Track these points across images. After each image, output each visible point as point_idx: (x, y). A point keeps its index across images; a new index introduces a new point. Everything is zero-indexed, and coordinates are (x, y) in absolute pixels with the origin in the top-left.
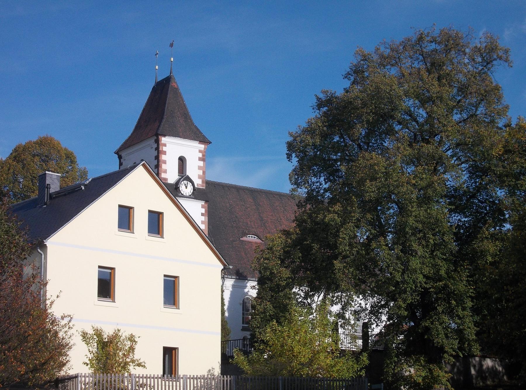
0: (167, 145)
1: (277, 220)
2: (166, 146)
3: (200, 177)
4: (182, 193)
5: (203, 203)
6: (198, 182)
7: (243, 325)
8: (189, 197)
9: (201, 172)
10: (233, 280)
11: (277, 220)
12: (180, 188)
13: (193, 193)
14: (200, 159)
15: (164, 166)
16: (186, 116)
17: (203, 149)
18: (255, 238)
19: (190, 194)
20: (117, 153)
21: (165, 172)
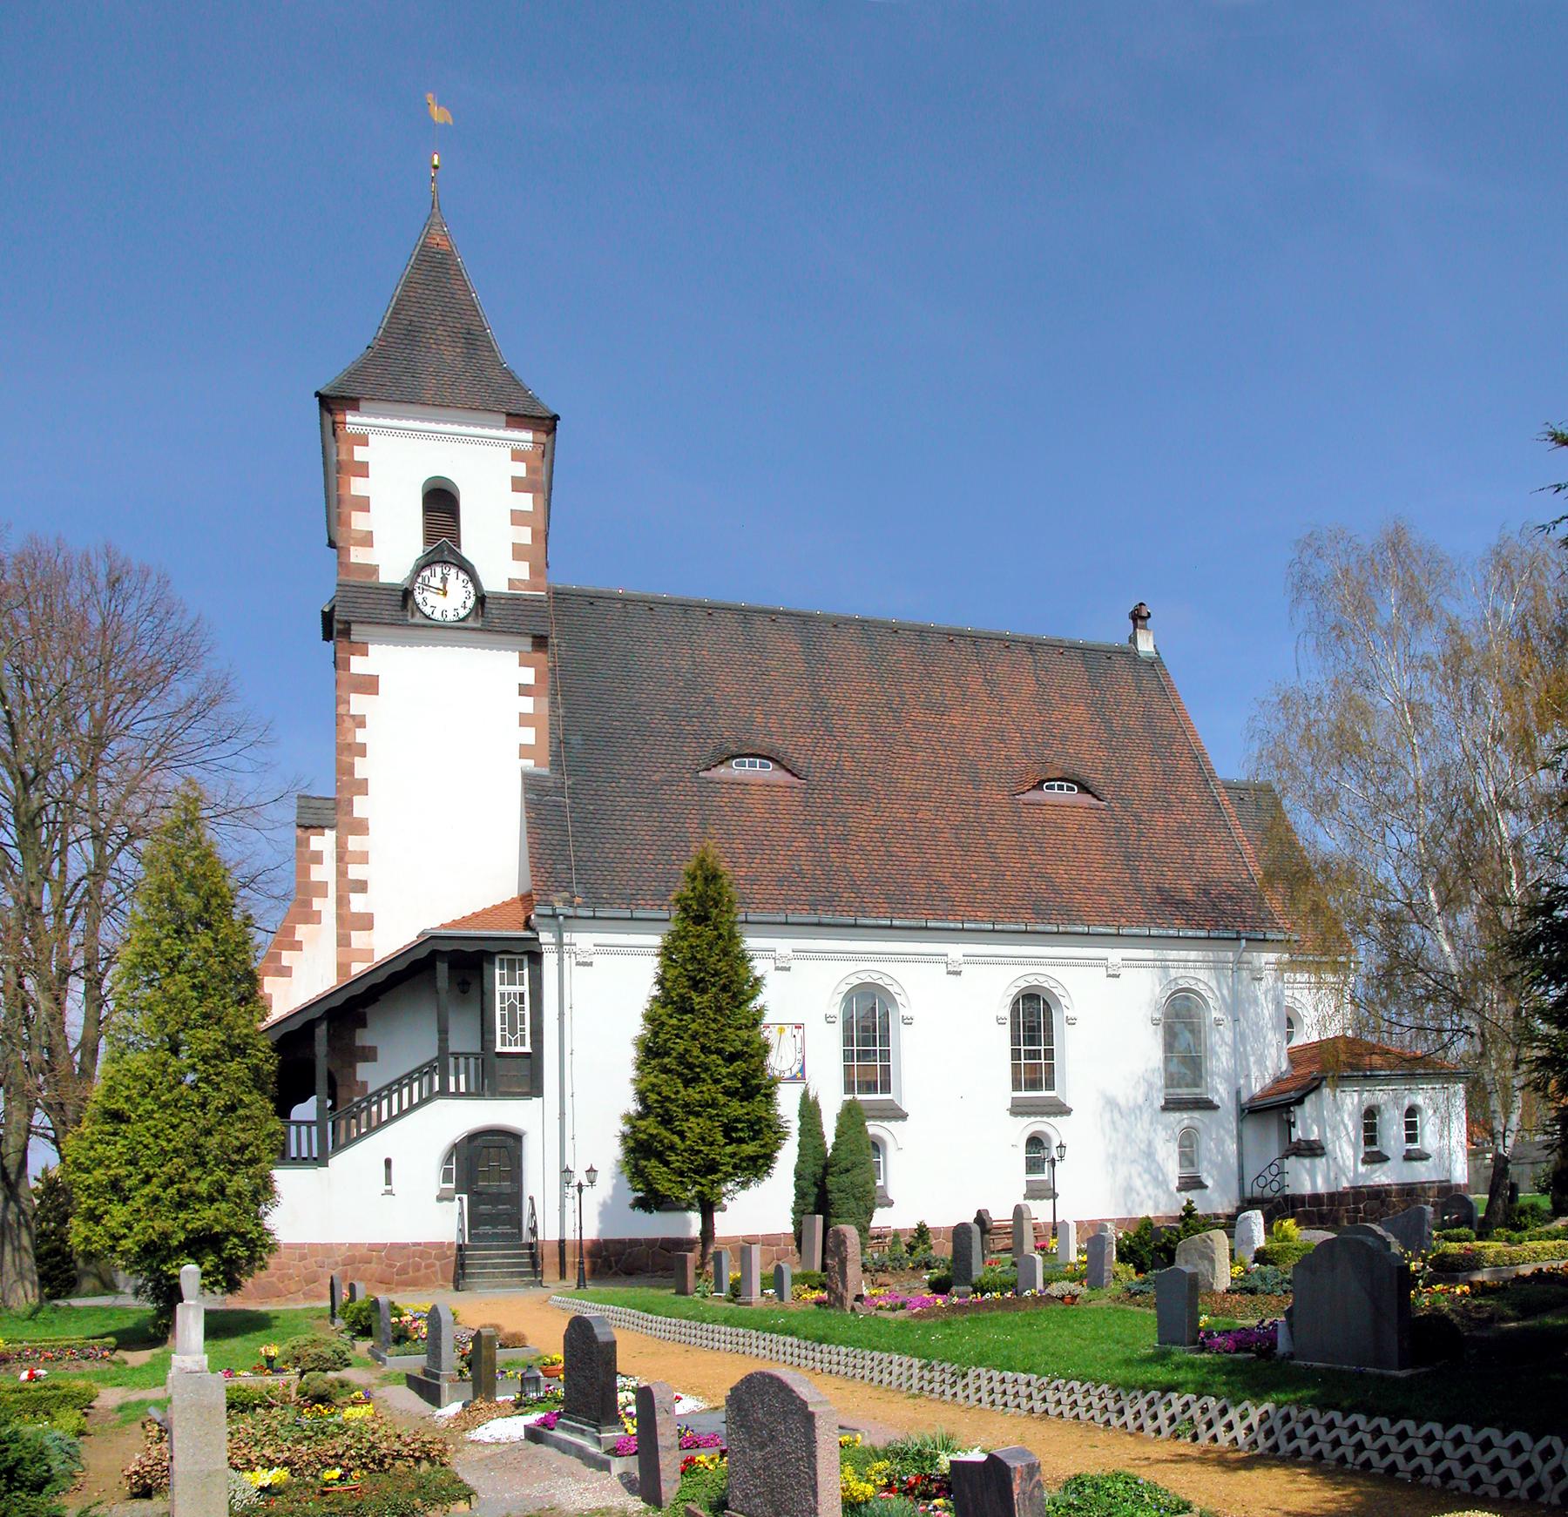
4: (427, 610)
16: (474, 340)
19: (463, 613)
21: (367, 540)
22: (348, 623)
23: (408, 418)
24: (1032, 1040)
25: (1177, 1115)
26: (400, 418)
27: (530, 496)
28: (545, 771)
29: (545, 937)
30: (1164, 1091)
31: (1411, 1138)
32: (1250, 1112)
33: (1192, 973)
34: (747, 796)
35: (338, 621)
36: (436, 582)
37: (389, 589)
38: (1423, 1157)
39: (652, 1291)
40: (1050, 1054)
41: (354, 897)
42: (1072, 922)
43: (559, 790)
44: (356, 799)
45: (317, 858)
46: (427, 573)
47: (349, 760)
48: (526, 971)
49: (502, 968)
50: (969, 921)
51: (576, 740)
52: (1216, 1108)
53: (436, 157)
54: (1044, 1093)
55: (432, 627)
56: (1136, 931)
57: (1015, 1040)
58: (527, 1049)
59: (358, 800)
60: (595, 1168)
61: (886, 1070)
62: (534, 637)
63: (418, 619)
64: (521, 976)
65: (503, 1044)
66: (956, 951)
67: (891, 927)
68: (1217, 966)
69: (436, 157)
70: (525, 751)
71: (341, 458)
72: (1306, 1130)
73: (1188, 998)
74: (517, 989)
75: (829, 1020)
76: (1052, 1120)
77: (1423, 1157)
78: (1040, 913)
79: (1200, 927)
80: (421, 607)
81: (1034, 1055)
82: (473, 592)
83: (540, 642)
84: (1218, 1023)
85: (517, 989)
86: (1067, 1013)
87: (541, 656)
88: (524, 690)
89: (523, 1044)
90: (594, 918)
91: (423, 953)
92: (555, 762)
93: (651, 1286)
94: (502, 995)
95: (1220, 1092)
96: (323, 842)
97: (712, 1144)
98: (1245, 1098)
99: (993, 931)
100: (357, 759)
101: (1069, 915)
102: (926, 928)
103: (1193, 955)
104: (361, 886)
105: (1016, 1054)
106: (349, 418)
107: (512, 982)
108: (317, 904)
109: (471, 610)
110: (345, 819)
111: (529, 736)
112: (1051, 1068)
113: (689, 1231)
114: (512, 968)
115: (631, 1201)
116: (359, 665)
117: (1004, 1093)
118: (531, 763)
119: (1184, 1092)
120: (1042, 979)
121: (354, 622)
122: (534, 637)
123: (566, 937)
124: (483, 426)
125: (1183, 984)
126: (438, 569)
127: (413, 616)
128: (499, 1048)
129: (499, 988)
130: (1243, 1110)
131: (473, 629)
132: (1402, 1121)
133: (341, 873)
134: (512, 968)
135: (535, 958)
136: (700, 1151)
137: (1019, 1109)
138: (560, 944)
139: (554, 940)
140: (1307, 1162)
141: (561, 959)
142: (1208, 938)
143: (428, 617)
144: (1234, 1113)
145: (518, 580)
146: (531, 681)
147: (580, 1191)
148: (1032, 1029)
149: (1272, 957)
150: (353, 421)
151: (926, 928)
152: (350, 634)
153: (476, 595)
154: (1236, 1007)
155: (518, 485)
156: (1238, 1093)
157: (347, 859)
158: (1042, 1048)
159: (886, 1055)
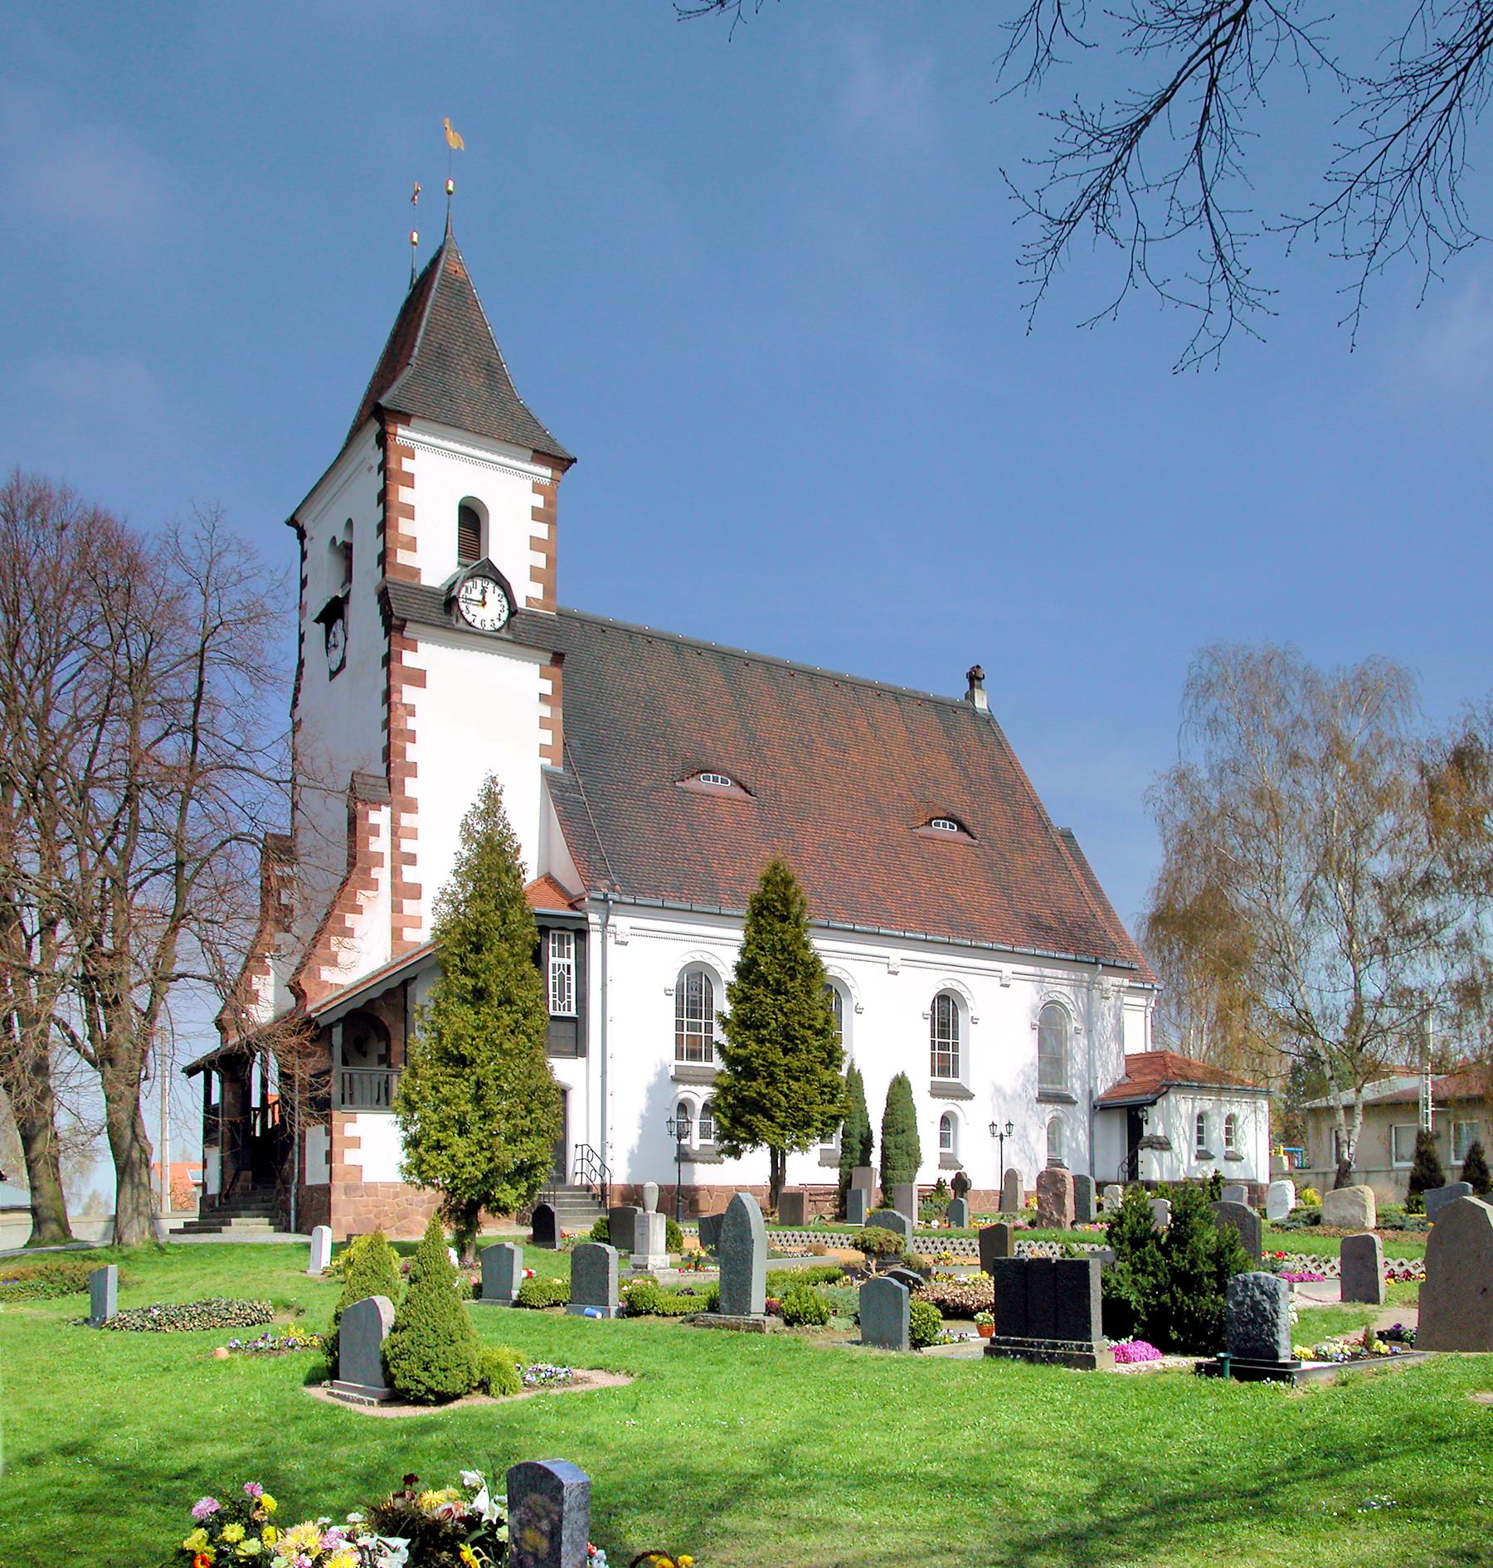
0: (417, 452)
1: (801, 740)
2: (413, 457)
3: (535, 574)
4: (470, 618)
6: (526, 591)
7: (934, 1079)
9: (540, 560)
11: (801, 740)
13: (508, 622)
14: (537, 515)
15: (405, 527)
16: (492, 371)
19: (498, 624)
20: (292, 522)
21: (411, 545)
22: (405, 620)
23: (481, 449)
24: (694, 1013)
25: (1050, 1107)
26: (443, 438)
28: (560, 770)
29: (593, 918)
30: (1036, 1085)
31: (1228, 1142)
32: (1102, 1109)
33: (1058, 988)
34: (1275, 938)
35: (397, 618)
36: (476, 595)
37: (430, 592)
38: (1238, 1158)
41: (405, 868)
42: (978, 938)
43: (576, 788)
44: (408, 780)
46: (469, 584)
47: (402, 744)
48: (572, 946)
49: (554, 942)
51: (575, 742)
52: (1075, 1103)
53: (451, 183)
54: (951, 1080)
55: (475, 634)
57: (679, 1012)
58: (573, 1013)
62: (555, 654)
63: (461, 625)
64: (569, 949)
65: (555, 1009)
66: (896, 954)
67: (853, 931)
68: (1077, 985)
69: (451, 183)
70: (544, 750)
72: (1155, 1129)
73: (1054, 1008)
74: (565, 961)
76: (959, 1102)
77: (1238, 1158)
78: (954, 929)
79: (1066, 951)
82: (506, 607)
83: (558, 658)
84: (1077, 1030)
85: (565, 961)
86: (971, 1013)
87: (557, 671)
88: (543, 698)
89: (569, 1010)
90: (634, 904)
92: (567, 764)
94: (554, 965)
95: (1076, 1088)
96: (380, 817)
97: (811, 1103)
98: (1095, 1097)
99: (926, 940)
100: (409, 745)
101: (972, 930)
102: (878, 934)
103: (1060, 973)
104: (412, 859)
105: (679, 1025)
106: (400, 431)
107: (561, 956)
108: (375, 873)
110: (399, 797)
111: (547, 737)
112: (955, 1058)
113: (692, 1178)
114: (561, 943)
116: (409, 659)
118: (548, 762)
119: (1050, 1088)
120: (706, 956)
121: (411, 620)
122: (555, 654)
123: (612, 919)
124: (511, 457)
125: (1054, 996)
126: (479, 582)
127: (457, 621)
128: (552, 1012)
129: (552, 960)
130: (1095, 1107)
131: (508, 640)
132: (1224, 1127)
133: (395, 846)
134: (561, 943)
135: (582, 934)
136: (802, 1109)
138: (605, 925)
139: (599, 921)
140: (1157, 1153)
141: (604, 939)
142: (1076, 961)
143: (470, 624)
144: (1086, 1108)
146: (549, 692)
147: (1001, 1139)
148: (694, 1003)
149: (1117, 980)
150: (403, 434)
151: (878, 934)
153: (509, 609)
154: (1089, 1018)
156: (1091, 1092)
158: (703, 1021)
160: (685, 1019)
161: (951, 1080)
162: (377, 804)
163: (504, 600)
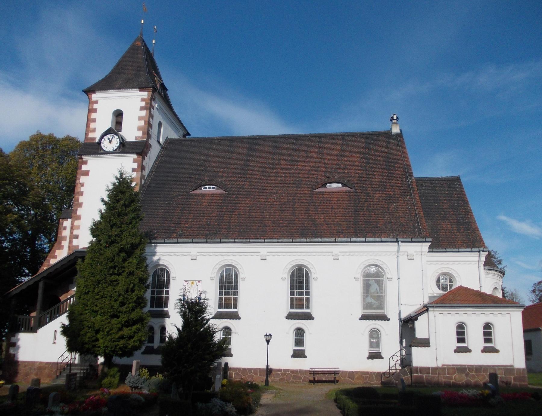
5: (135, 156)
8: (114, 152)
10: (426, 245)
12: (102, 144)
15: (142, 123)
17: (146, 97)
18: (215, 188)
27: (145, 111)
39: (364, 386)
40: (308, 293)
45: (65, 228)
47: (78, 197)
50: (267, 239)
54: (232, 310)
56: (241, 240)
57: (292, 287)
59: (79, 209)
60: (271, 334)
61: (236, 300)
63: (102, 151)
71: (90, 108)
75: (283, 279)
80: (103, 148)
81: (228, 293)
91: (73, 257)
93: (57, 384)
104: (77, 237)
109: (118, 147)
110: (75, 215)
115: (455, 348)
117: (286, 309)
127: (100, 151)
133: (71, 233)
137: (290, 316)
143: (104, 151)
145: (138, 137)
150: (94, 97)
152: (82, 158)
155: (142, 108)
157: (74, 228)
158: (304, 291)
159: (236, 293)
160: (224, 290)
161: (232, 310)
162: (66, 218)
163: (118, 139)
